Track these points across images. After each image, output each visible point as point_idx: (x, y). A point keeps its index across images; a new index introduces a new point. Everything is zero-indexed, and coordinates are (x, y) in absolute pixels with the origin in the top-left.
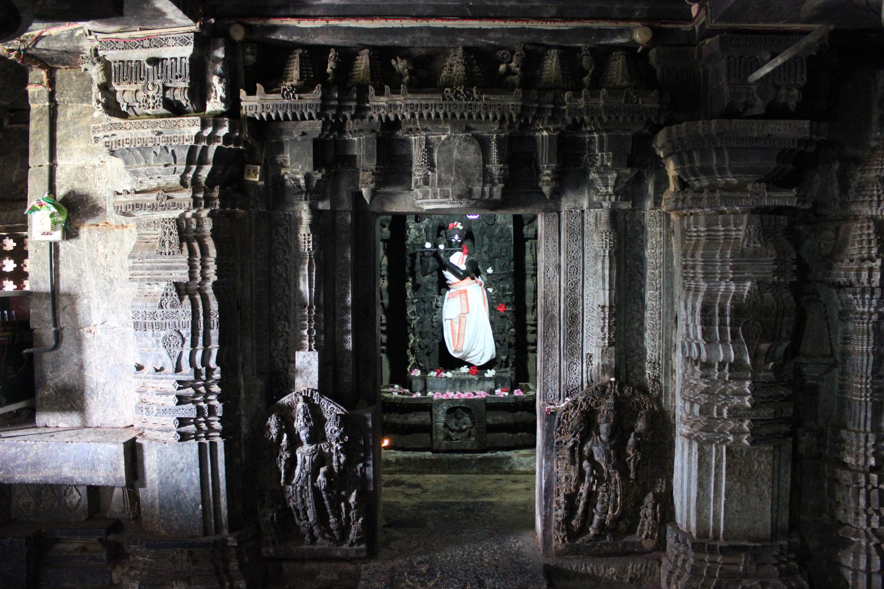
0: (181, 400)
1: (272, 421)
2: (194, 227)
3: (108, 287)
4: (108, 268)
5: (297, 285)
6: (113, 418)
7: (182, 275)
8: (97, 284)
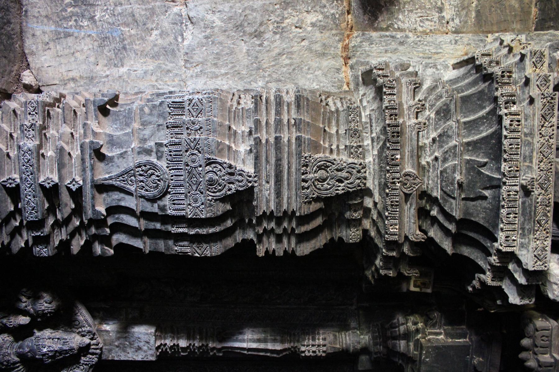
0: (51, 193)
1: (46, 304)
2: (348, 215)
3: (248, 29)
4: (280, 31)
5: (253, 322)
6: (38, 33)
7: (266, 199)
8: (253, 10)
